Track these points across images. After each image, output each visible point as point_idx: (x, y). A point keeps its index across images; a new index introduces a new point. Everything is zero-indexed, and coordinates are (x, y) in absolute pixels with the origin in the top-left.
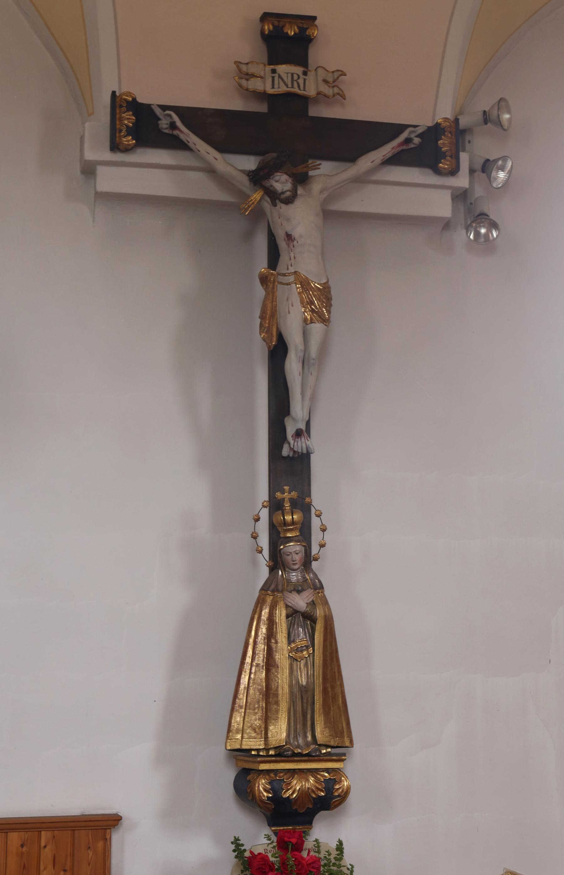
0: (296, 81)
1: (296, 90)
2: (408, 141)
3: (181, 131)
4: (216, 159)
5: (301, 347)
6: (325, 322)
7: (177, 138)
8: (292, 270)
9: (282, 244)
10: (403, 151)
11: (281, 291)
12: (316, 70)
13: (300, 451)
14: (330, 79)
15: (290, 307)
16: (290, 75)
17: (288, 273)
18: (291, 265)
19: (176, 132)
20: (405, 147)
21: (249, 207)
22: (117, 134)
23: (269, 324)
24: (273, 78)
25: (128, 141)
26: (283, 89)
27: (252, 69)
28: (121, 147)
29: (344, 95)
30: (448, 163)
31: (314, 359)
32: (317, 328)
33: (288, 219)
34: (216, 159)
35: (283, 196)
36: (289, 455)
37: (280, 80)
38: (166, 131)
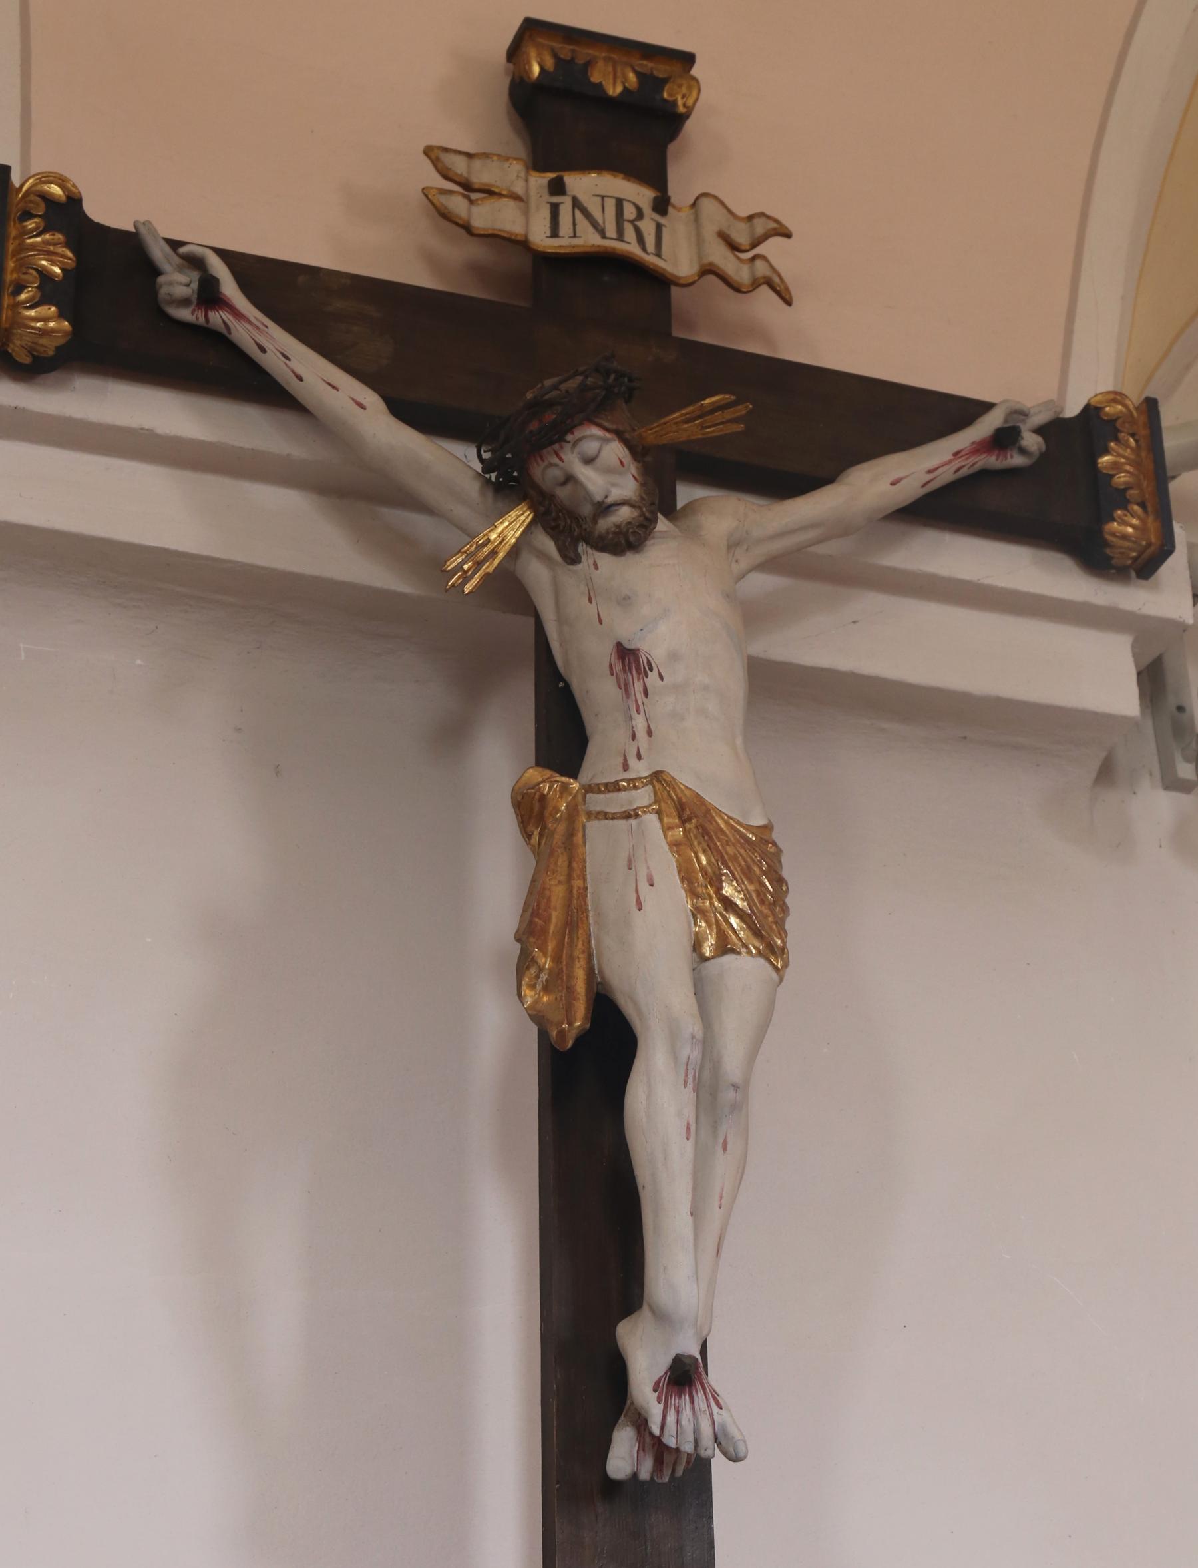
0: (631, 222)
1: (630, 247)
2: (1005, 438)
3: (237, 314)
4: (362, 407)
5: (691, 1026)
6: (774, 953)
7: (221, 340)
8: (641, 769)
9: (597, 692)
10: (984, 475)
11: (599, 841)
12: (694, 205)
13: (688, 1448)
14: (741, 236)
15: (643, 885)
16: (610, 206)
17: (628, 781)
18: (639, 757)
19: (217, 318)
20: (992, 461)
21: (478, 564)
22: (7, 301)
23: (557, 959)
24: (555, 209)
25: (46, 320)
26: (589, 239)
27: (483, 175)
28: (18, 350)
29: (787, 289)
30: (1135, 521)
31: (736, 1087)
32: (744, 971)
33: (627, 598)
34: (362, 407)
35: (605, 524)
36: (635, 1475)
37: (577, 212)
38: (184, 314)
